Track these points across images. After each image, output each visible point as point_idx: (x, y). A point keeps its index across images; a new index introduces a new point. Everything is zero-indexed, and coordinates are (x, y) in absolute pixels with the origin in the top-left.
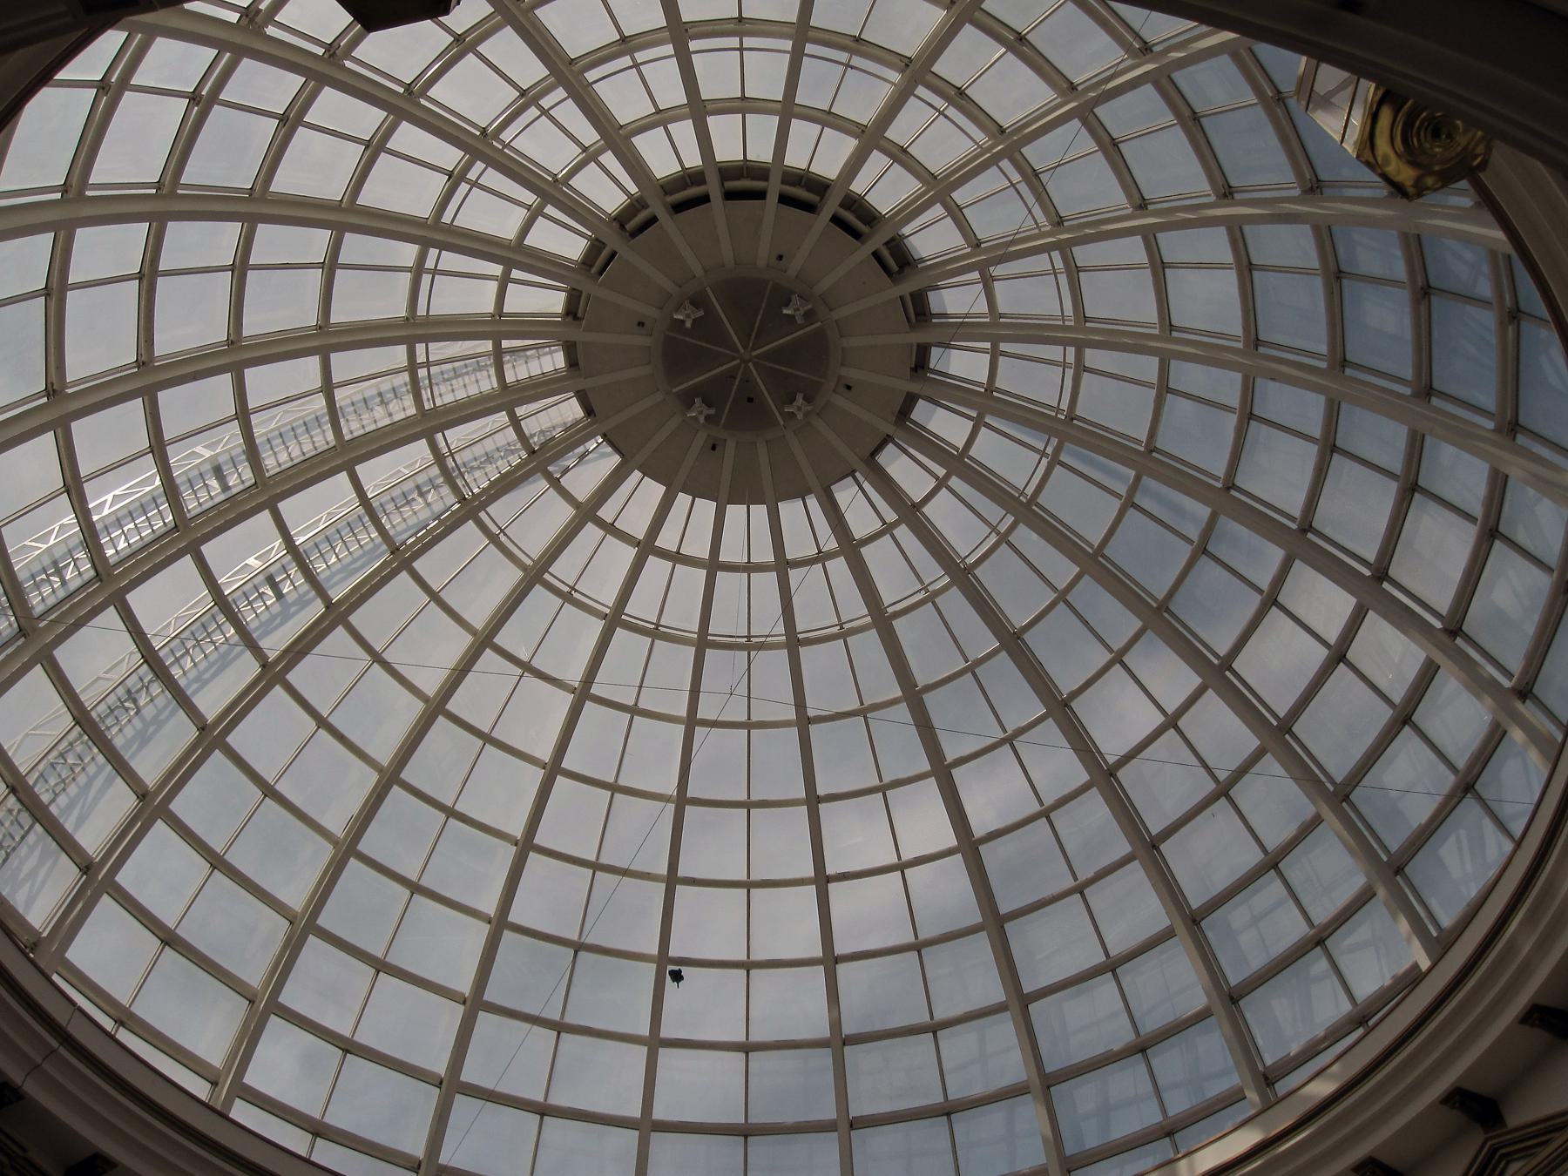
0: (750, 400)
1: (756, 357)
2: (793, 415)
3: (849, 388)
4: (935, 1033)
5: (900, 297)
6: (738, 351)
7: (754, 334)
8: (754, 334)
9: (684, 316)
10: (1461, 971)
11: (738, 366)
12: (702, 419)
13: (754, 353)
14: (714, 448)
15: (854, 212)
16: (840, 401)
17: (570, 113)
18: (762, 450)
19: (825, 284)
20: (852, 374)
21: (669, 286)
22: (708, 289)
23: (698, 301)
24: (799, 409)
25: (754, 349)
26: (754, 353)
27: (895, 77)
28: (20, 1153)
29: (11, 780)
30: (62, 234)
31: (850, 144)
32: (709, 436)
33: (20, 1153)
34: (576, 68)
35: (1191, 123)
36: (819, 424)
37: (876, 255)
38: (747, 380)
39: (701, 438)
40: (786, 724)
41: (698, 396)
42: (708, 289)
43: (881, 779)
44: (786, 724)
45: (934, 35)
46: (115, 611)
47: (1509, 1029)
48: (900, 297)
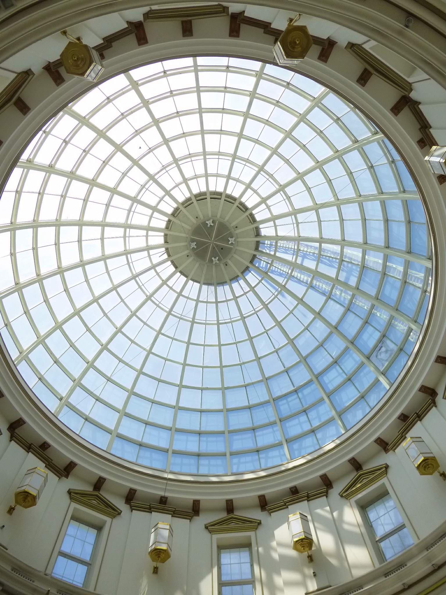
1: (214, 240)
4: (202, 390)
7: (209, 236)
8: (209, 236)
9: (193, 245)
10: (147, 204)
11: (212, 245)
12: (218, 262)
14: (226, 265)
15: (202, 196)
16: (238, 231)
17: (133, 232)
19: (210, 214)
20: (234, 224)
23: (193, 241)
25: (212, 239)
28: (51, 461)
29: (39, 377)
30: (19, 292)
33: (51, 461)
36: (240, 240)
37: (211, 198)
38: (217, 246)
40: (165, 311)
41: (212, 257)
44: (165, 311)
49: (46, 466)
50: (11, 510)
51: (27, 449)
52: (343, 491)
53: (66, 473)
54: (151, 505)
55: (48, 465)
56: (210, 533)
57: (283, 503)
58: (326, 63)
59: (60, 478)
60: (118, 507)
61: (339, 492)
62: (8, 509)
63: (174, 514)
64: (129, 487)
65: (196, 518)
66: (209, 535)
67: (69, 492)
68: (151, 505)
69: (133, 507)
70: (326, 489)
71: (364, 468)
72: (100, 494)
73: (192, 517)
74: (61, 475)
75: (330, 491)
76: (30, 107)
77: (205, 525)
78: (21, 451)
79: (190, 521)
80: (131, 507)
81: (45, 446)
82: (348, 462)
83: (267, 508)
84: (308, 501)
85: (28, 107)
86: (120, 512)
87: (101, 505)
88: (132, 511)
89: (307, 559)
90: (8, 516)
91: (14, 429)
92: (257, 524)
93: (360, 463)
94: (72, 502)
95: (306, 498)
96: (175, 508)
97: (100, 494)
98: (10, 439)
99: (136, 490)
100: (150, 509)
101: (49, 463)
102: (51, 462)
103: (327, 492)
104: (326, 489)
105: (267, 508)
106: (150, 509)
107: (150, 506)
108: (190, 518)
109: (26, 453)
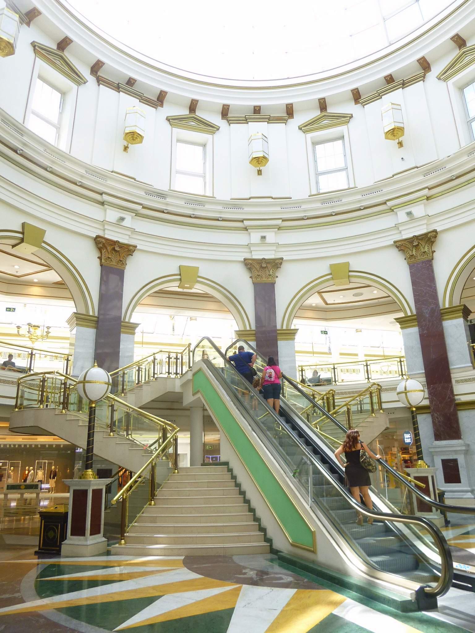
28: (142, 95)
33: (142, 95)
49: (140, 101)
50: (126, 148)
51: (117, 90)
52: (441, 74)
53: (160, 103)
54: (246, 117)
55: (142, 99)
56: (304, 133)
57: (377, 94)
58: (457, 459)
59: (156, 108)
60: (214, 123)
61: (436, 75)
62: (123, 148)
63: (269, 120)
64: (222, 103)
65: (290, 121)
66: (303, 135)
67: (168, 119)
68: (246, 117)
69: (230, 122)
70: (423, 73)
71: (468, 44)
72: (196, 115)
73: (287, 120)
74: (156, 105)
75: (428, 75)
76: (65, 36)
77: (299, 127)
78: (112, 93)
79: (286, 124)
80: (228, 121)
81: (131, 82)
82: (450, 40)
83: (360, 101)
84: (403, 89)
85: (65, 38)
86: (218, 128)
87: (200, 125)
88: (230, 125)
89: (397, 146)
90: (124, 153)
91: (97, 73)
92: (349, 118)
93: (464, 38)
94: (173, 128)
95: (402, 85)
96: (270, 115)
97: (196, 115)
98: (97, 84)
99: (229, 105)
100: (246, 120)
101: (141, 97)
102: (144, 96)
103: (424, 77)
104: (423, 73)
105: (360, 101)
106: (246, 120)
107: (245, 117)
108: (285, 121)
109: (117, 93)
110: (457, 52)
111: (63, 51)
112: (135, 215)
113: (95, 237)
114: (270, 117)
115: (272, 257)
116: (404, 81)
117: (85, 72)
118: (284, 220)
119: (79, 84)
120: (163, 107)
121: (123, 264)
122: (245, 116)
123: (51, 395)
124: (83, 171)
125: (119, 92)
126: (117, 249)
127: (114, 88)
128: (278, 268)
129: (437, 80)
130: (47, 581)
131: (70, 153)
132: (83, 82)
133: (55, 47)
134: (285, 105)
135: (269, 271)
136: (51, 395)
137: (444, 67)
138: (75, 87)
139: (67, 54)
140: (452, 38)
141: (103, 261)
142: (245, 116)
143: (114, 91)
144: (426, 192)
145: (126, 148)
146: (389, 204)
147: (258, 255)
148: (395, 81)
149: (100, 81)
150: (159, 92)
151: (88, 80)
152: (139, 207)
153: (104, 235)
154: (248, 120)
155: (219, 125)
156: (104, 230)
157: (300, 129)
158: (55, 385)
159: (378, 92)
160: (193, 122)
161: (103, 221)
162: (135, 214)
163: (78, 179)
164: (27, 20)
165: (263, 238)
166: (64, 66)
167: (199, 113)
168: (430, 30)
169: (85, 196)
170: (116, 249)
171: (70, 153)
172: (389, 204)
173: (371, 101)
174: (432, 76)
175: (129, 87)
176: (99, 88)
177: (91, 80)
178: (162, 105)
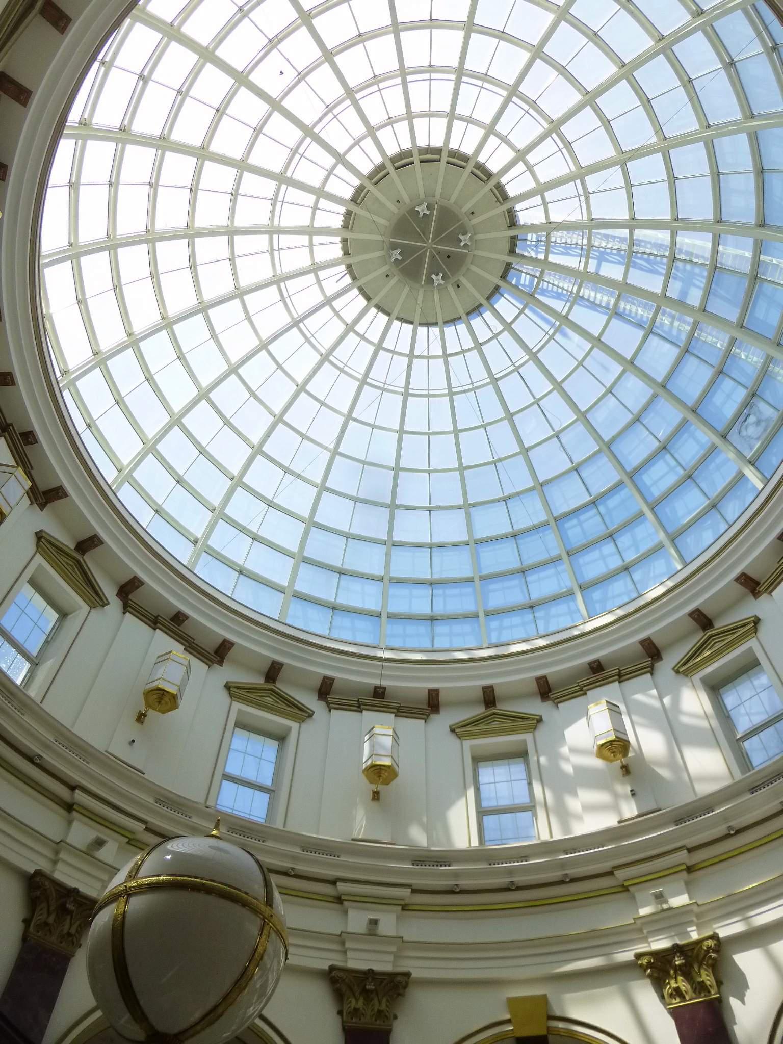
0: (448, 257)
2: (466, 245)
3: (472, 213)
5: (420, 162)
6: (425, 247)
7: (422, 235)
8: (422, 235)
9: (396, 255)
11: (431, 251)
12: (442, 282)
13: (430, 241)
14: (458, 287)
15: (404, 158)
16: (475, 221)
18: (474, 268)
21: (379, 254)
22: (391, 240)
23: (394, 246)
24: (465, 240)
25: (428, 240)
26: (430, 241)
27: (546, 125)
31: (369, 139)
32: (452, 285)
34: (230, 226)
35: (594, 38)
36: (479, 237)
39: (451, 289)
42: (391, 240)
43: (429, 430)
45: (569, 111)
46: (603, 437)
47: (633, 643)
48: (420, 162)
50: (141, 718)
51: (152, 625)
53: (218, 658)
56: (459, 738)
62: (136, 715)
67: (228, 687)
68: (360, 700)
69: (331, 705)
70: (650, 662)
75: (658, 665)
79: (425, 722)
80: (328, 705)
81: (179, 618)
88: (330, 711)
95: (617, 677)
100: (359, 706)
102: (193, 643)
104: (650, 662)
106: (359, 706)
107: (358, 701)
108: (425, 717)
110: (699, 637)
111: (83, 554)
112: (128, 843)
113: (32, 872)
114: (400, 706)
115: (387, 968)
116: (620, 671)
117: (110, 592)
118: (414, 891)
119: (92, 606)
120: (222, 666)
121: (73, 943)
122: (359, 699)
123: (684, 293)
124: (50, 737)
125: (155, 629)
126: (71, 906)
127: (149, 623)
128: (399, 994)
129: (673, 673)
130: (34, 348)
131: (41, 702)
132: (101, 604)
133: (73, 546)
134: (427, 691)
135: (380, 1002)
136: (684, 293)
137: (682, 656)
138: (86, 608)
139: (90, 561)
140: (737, 579)
141: (31, 929)
142: (359, 699)
143: (148, 627)
144: (683, 856)
145: (141, 718)
146: (620, 874)
147: (357, 962)
148: (604, 671)
149: (127, 607)
150: (221, 641)
151: (109, 600)
152: (139, 827)
153: (53, 871)
154: (362, 707)
155: (313, 709)
156: (55, 863)
157: (453, 731)
158: (693, 226)
159: (579, 684)
160: (269, 697)
161: (61, 841)
162: (127, 840)
163: (36, 749)
164: (42, 498)
165: (374, 922)
166: (77, 574)
167: (282, 686)
168: (738, 534)
169: (40, 785)
170: (68, 906)
171: (41, 702)
172: (620, 874)
173: (569, 697)
174: (666, 666)
175: (173, 626)
176: (123, 618)
177: (115, 604)
178: (221, 663)
